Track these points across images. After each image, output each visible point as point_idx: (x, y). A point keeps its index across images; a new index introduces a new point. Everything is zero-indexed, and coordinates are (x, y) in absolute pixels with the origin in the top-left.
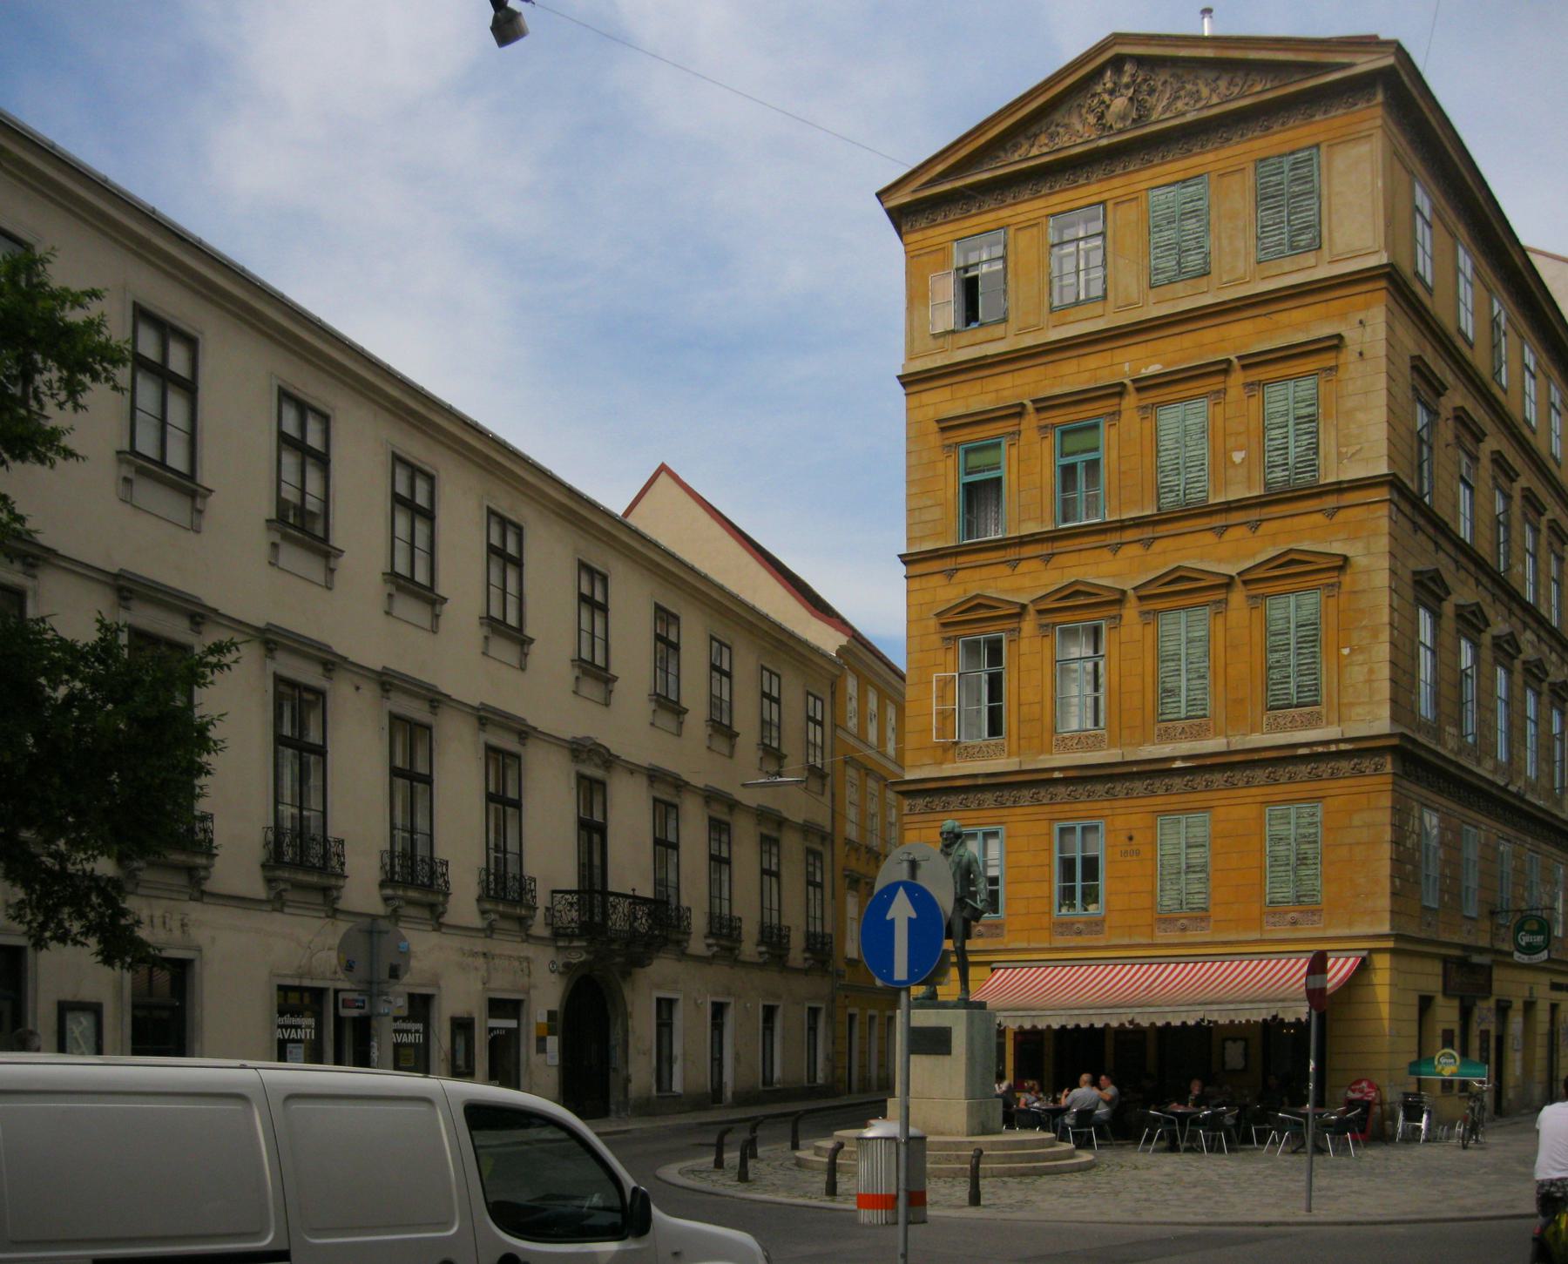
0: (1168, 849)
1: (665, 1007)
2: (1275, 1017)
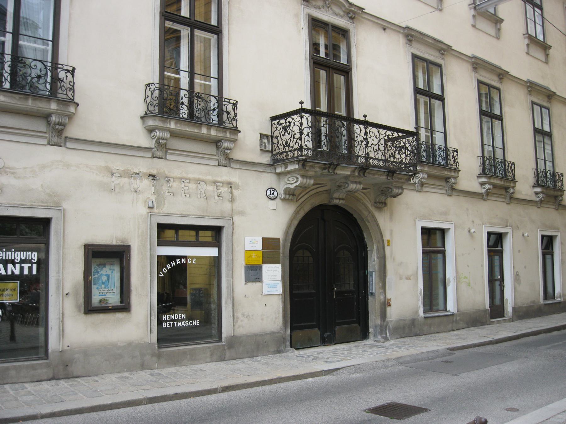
1: (433, 238)
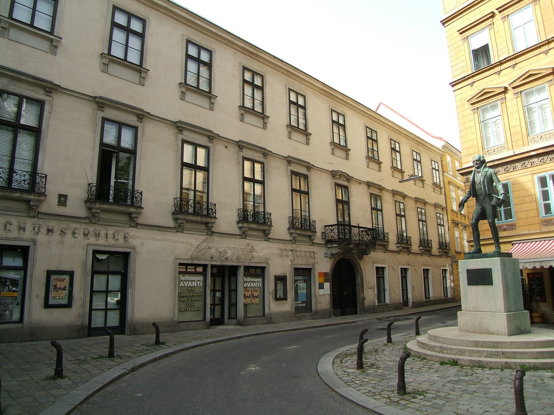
1: (380, 271)
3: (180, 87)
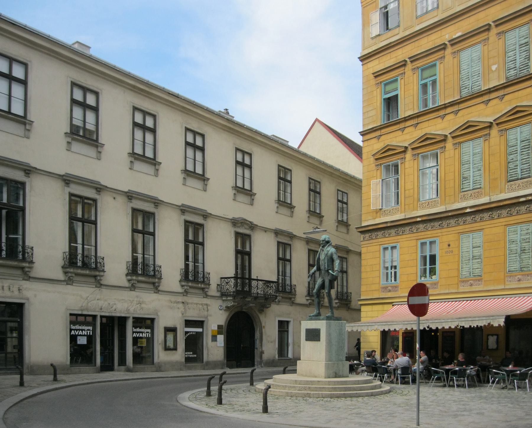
0: (465, 249)
1: (283, 326)
2: (489, 324)
3: (66, 136)
